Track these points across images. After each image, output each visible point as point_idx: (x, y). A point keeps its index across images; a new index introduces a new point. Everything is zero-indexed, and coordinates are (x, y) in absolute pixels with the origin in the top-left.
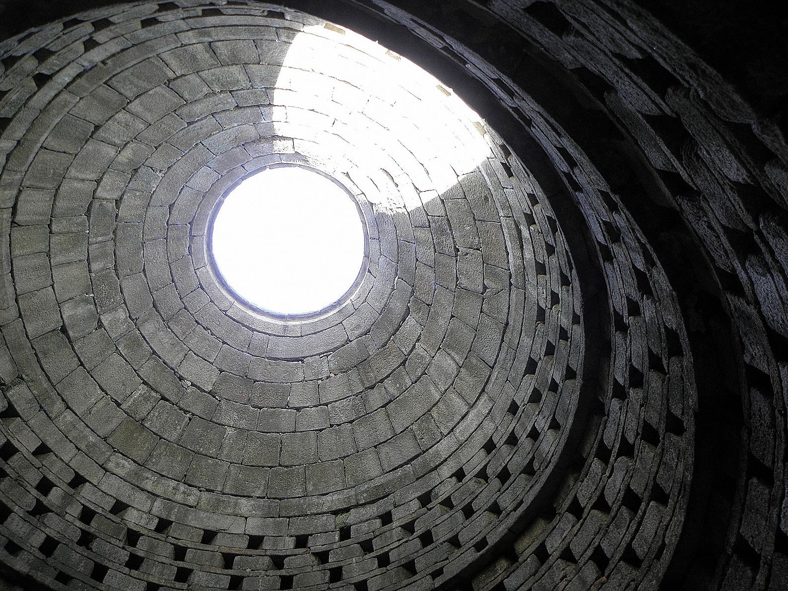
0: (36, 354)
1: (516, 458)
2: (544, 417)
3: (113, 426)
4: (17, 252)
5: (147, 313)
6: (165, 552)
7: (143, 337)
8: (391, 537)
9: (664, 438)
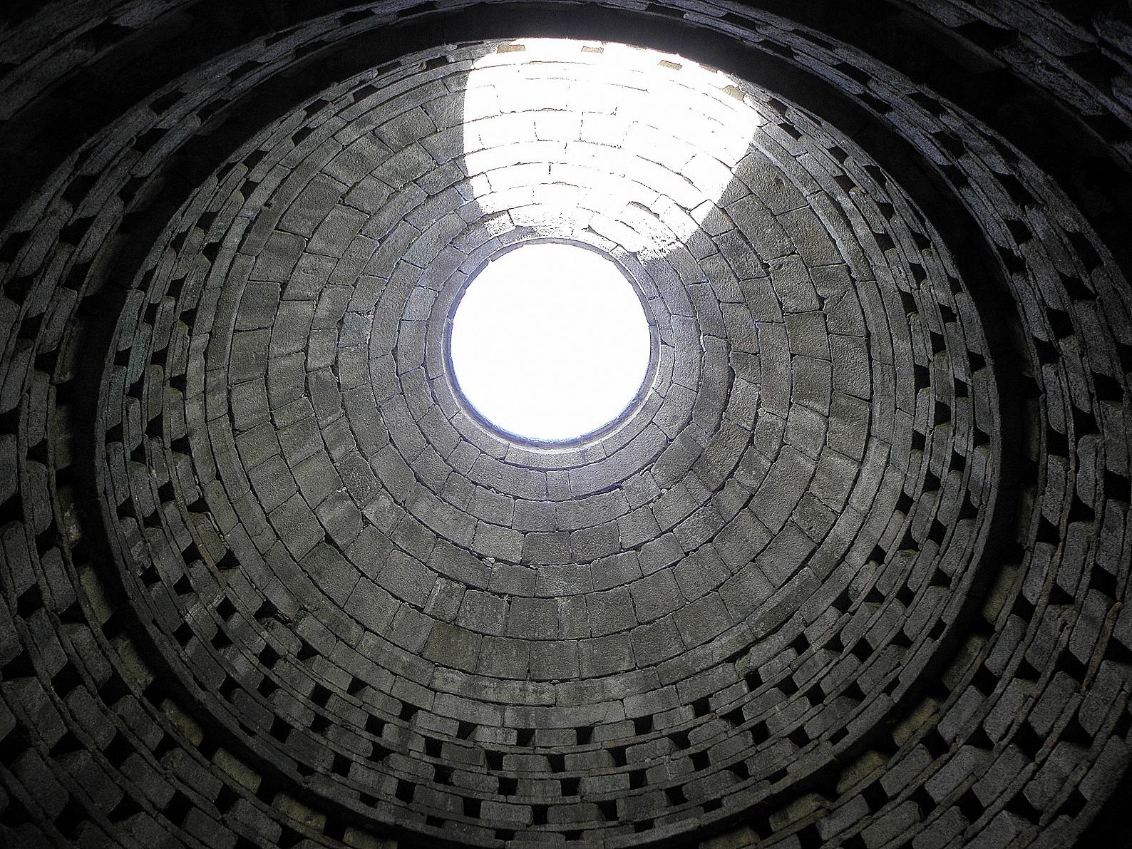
0: (309, 577)
1: (945, 503)
2: (963, 435)
3: (423, 636)
4: (249, 464)
5: (413, 491)
6: (539, 766)
7: (419, 521)
8: (815, 664)
9: (1126, 384)
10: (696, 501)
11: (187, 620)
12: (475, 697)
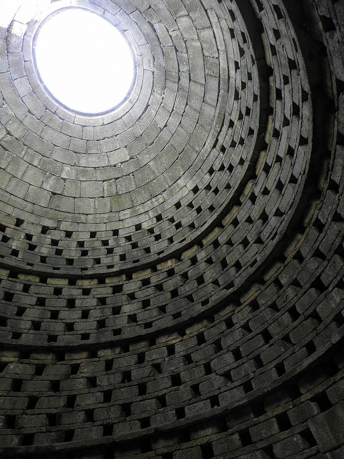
0: (55, 210)
7: (85, 167)
10: (175, 91)
11: (13, 248)
12: (137, 214)
